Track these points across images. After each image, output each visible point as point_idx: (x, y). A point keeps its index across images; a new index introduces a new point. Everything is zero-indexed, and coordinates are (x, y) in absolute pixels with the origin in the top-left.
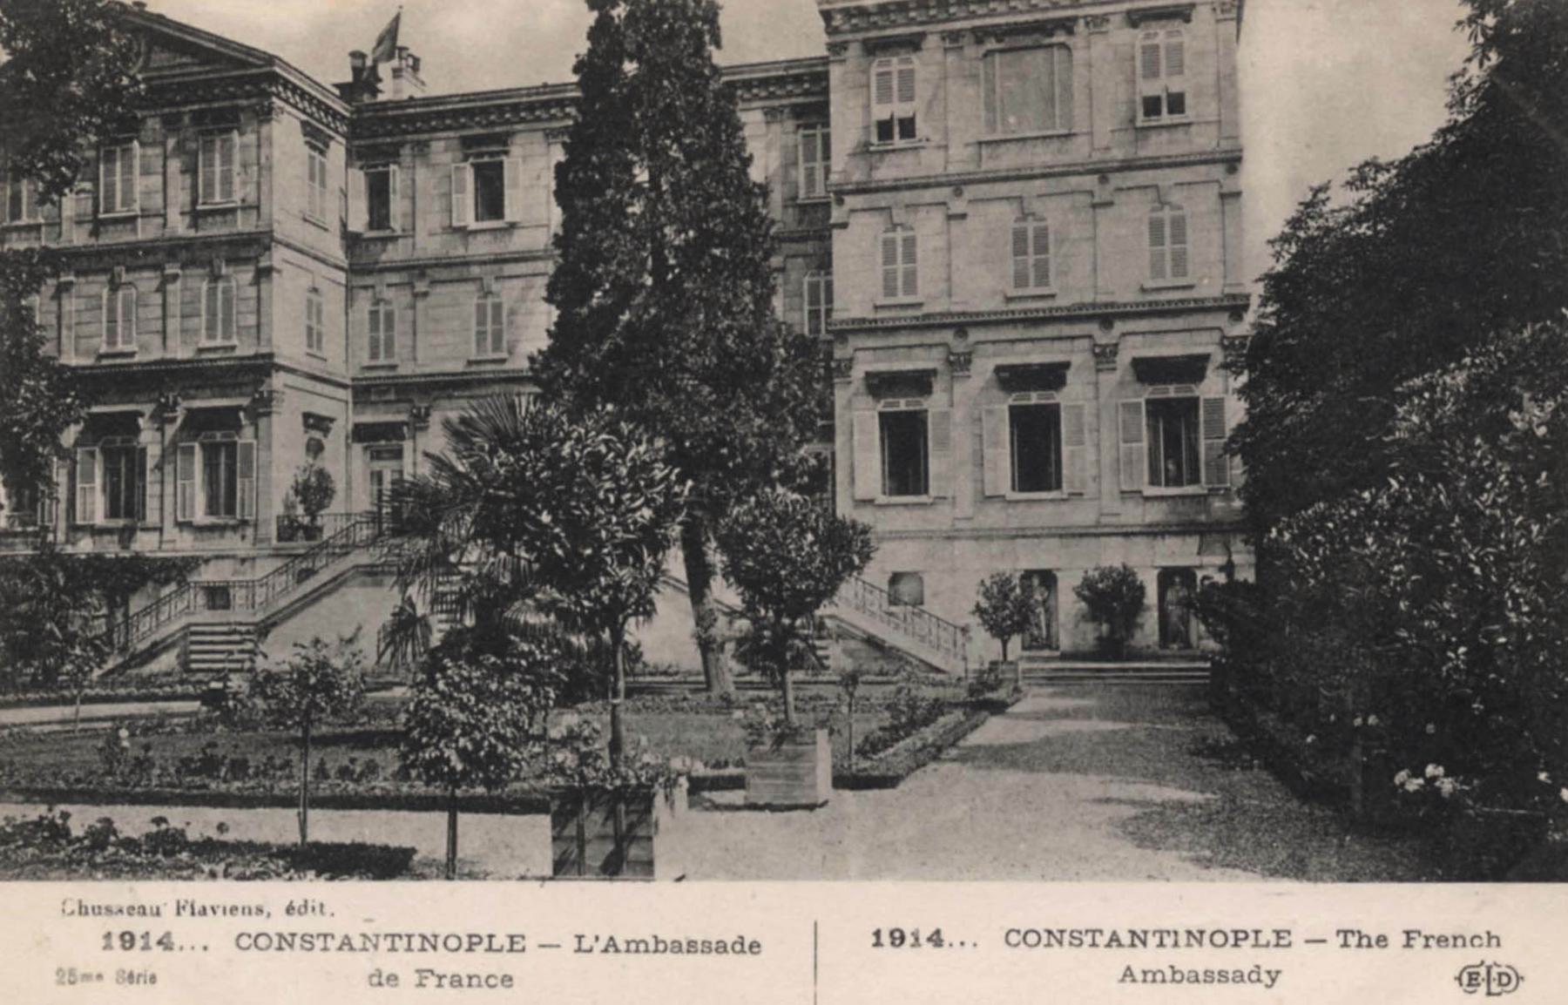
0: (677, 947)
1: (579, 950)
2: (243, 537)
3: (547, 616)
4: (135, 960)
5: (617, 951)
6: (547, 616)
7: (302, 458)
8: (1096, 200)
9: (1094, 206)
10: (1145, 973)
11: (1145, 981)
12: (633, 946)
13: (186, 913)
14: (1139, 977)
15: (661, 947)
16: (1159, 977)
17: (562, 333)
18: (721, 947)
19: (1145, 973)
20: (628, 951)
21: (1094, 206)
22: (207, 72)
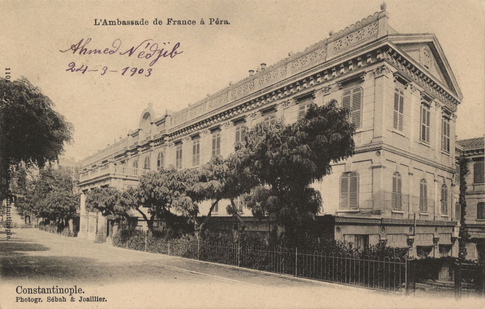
0: (124, 23)
1: (96, 24)
2: (421, 99)
3: (382, 243)
4: (79, 60)
5: (107, 24)
6: (382, 243)
7: (19, 229)
8: (374, 165)
9: (373, 168)
10: (110, 22)
11: (110, 24)
12: (111, 23)
13: (214, 23)
14: (108, 23)
15: (119, 23)
16: (114, 23)
17: (191, 197)
18: (137, 23)
19: (110, 22)
20: (110, 24)
21: (373, 168)
22: (440, 82)
